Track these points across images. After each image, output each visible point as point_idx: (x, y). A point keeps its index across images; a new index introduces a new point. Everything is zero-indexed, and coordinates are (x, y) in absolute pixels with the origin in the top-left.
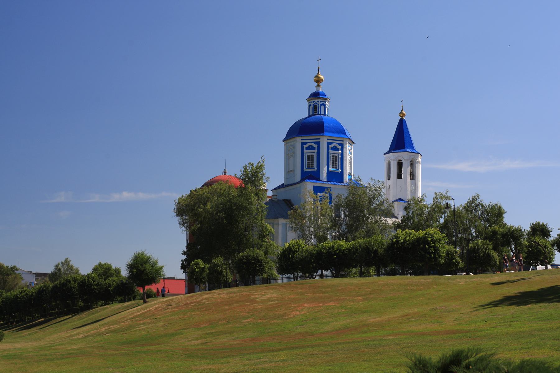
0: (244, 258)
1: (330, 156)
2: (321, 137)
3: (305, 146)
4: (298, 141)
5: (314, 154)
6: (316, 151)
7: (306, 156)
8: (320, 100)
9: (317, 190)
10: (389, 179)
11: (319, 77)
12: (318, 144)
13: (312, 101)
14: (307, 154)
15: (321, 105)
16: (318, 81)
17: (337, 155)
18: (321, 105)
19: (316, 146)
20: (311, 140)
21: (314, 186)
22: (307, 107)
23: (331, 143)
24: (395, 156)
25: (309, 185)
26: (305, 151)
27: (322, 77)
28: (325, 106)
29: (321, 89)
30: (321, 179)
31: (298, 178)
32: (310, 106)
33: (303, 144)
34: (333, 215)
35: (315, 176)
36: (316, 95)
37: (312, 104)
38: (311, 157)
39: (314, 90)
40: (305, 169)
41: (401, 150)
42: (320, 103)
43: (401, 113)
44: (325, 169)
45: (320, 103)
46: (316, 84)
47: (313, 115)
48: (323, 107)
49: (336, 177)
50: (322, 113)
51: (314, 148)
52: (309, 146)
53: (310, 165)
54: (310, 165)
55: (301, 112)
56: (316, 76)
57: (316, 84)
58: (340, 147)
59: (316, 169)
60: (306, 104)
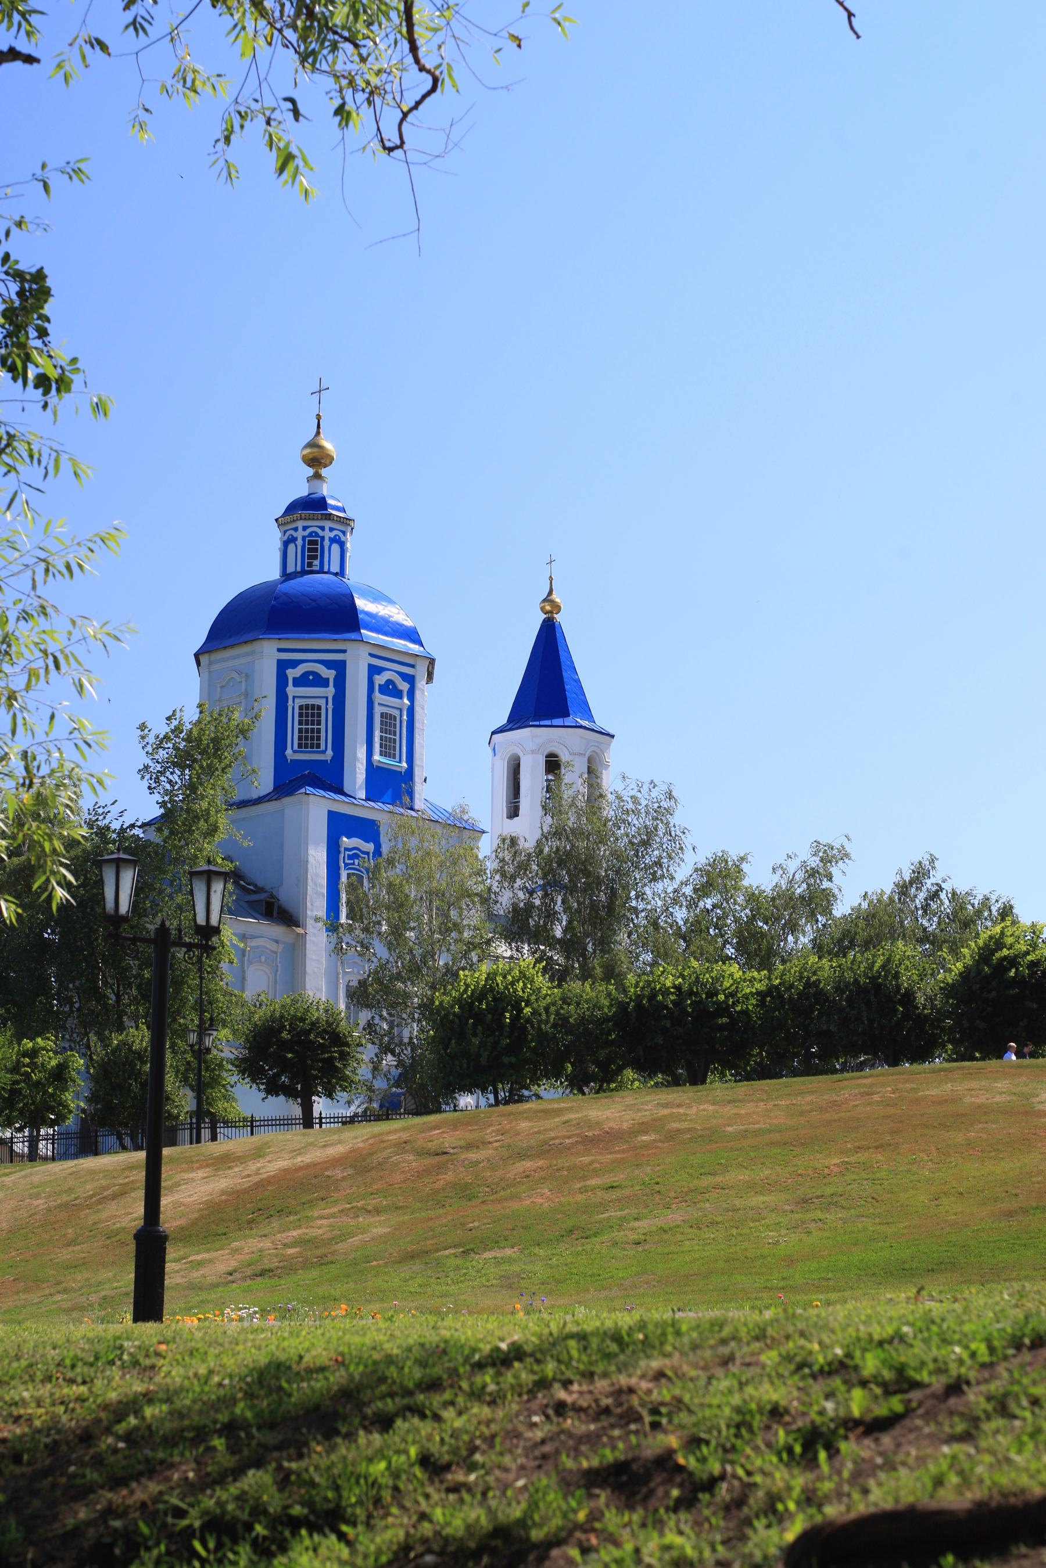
0: (821, 1056)
1: (378, 710)
2: (348, 646)
3: (292, 673)
4: (265, 655)
5: (322, 702)
6: (330, 691)
7: (293, 708)
8: (328, 524)
9: (340, 825)
10: (514, 812)
11: (321, 447)
12: (340, 667)
13: (300, 524)
14: (299, 702)
15: (333, 540)
16: (317, 459)
17: (396, 713)
18: (333, 540)
19: (330, 674)
20: (312, 650)
21: (331, 814)
22: (278, 545)
23: (379, 670)
24: (532, 742)
25: (315, 808)
26: (291, 690)
27: (328, 445)
28: (342, 545)
29: (325, 490)
30: (347, 789)
31: (265, 782)
32: (286, 544)
33: (282, 666)
34: (799, 891)
35: (329, 778)
36: (312, 506)
37: (300, 534)
38: (310, 713)
39: (302, 490)
40: (289, 752)
41: (556, 722)
42: (328, 535)
43: (548, 599)
44: (362, 753)
45: (328, 535)
46: (310, 472)
47: (304, 573)
48: (335, 548)
49: (393, 784)
50: (335, 568)
51: (323, 683)
52: (306, 674)
53: (309, 740)
54: (309, 740)
55: (259, 564)
56: (313, 444)
57: (310, 472)
58: (404, 687)
59: (330, 752)
60: (275, 537)
